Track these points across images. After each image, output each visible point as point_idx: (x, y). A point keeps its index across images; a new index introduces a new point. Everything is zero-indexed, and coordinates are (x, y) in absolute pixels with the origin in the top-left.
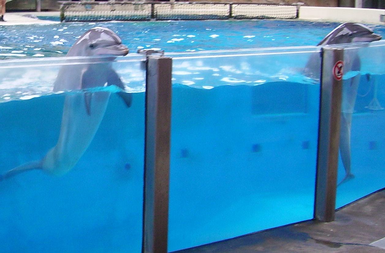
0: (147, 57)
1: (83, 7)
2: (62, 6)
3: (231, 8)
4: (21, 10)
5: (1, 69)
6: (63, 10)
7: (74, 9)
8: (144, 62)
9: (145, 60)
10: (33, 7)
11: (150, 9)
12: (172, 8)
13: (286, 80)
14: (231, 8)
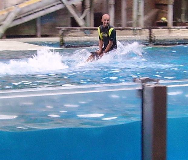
0: (143, 86)
1: (82, 33)
2: (61, 32)
3: (150, 32)
4: (20, 36)
5: (1, 93)
6: (63, 36)
7: (72, 34)
8: (140, 90)
9: (140, 88)
10: (32, 32)
11: (148, 35)
12: (170, 32)
13: (110, 119)
14: (150, 32)
